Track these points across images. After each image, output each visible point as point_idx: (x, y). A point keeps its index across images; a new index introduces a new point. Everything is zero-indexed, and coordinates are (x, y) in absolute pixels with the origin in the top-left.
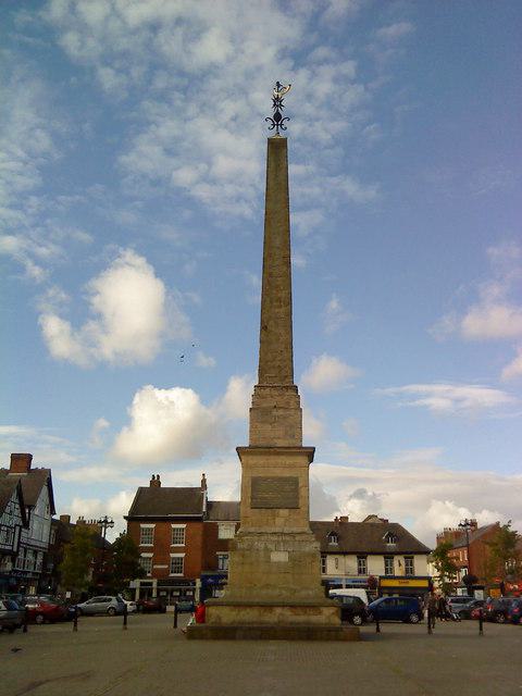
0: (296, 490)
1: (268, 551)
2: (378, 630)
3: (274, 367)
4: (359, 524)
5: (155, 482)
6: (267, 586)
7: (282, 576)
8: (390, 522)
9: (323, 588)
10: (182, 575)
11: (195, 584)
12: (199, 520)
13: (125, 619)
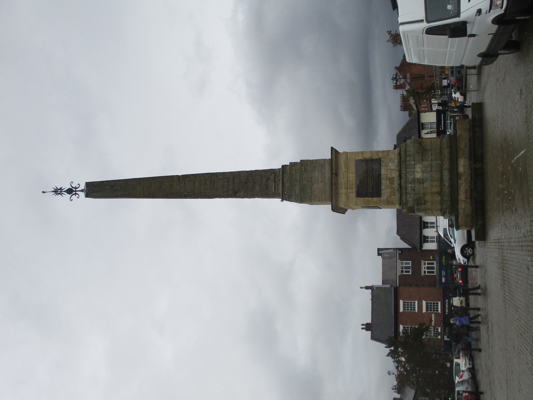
4: (406, 60)
5: (368, 327)
8: (400, 237)
12: (396, 289)
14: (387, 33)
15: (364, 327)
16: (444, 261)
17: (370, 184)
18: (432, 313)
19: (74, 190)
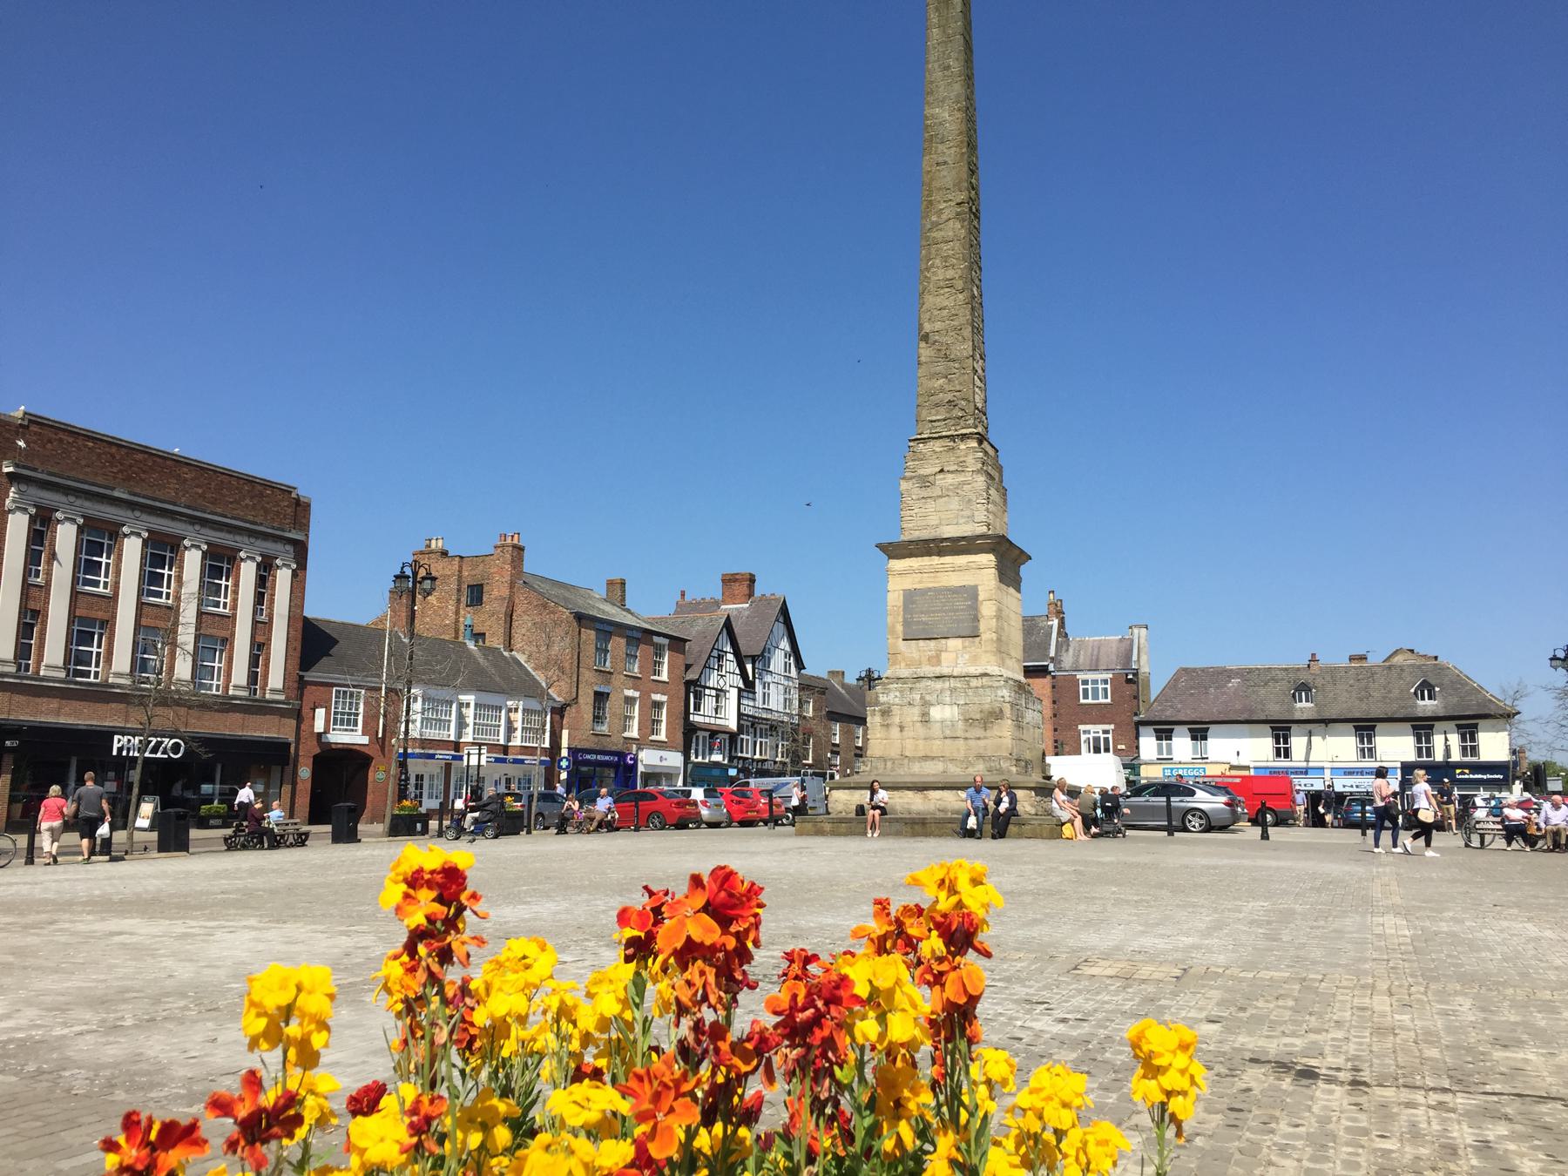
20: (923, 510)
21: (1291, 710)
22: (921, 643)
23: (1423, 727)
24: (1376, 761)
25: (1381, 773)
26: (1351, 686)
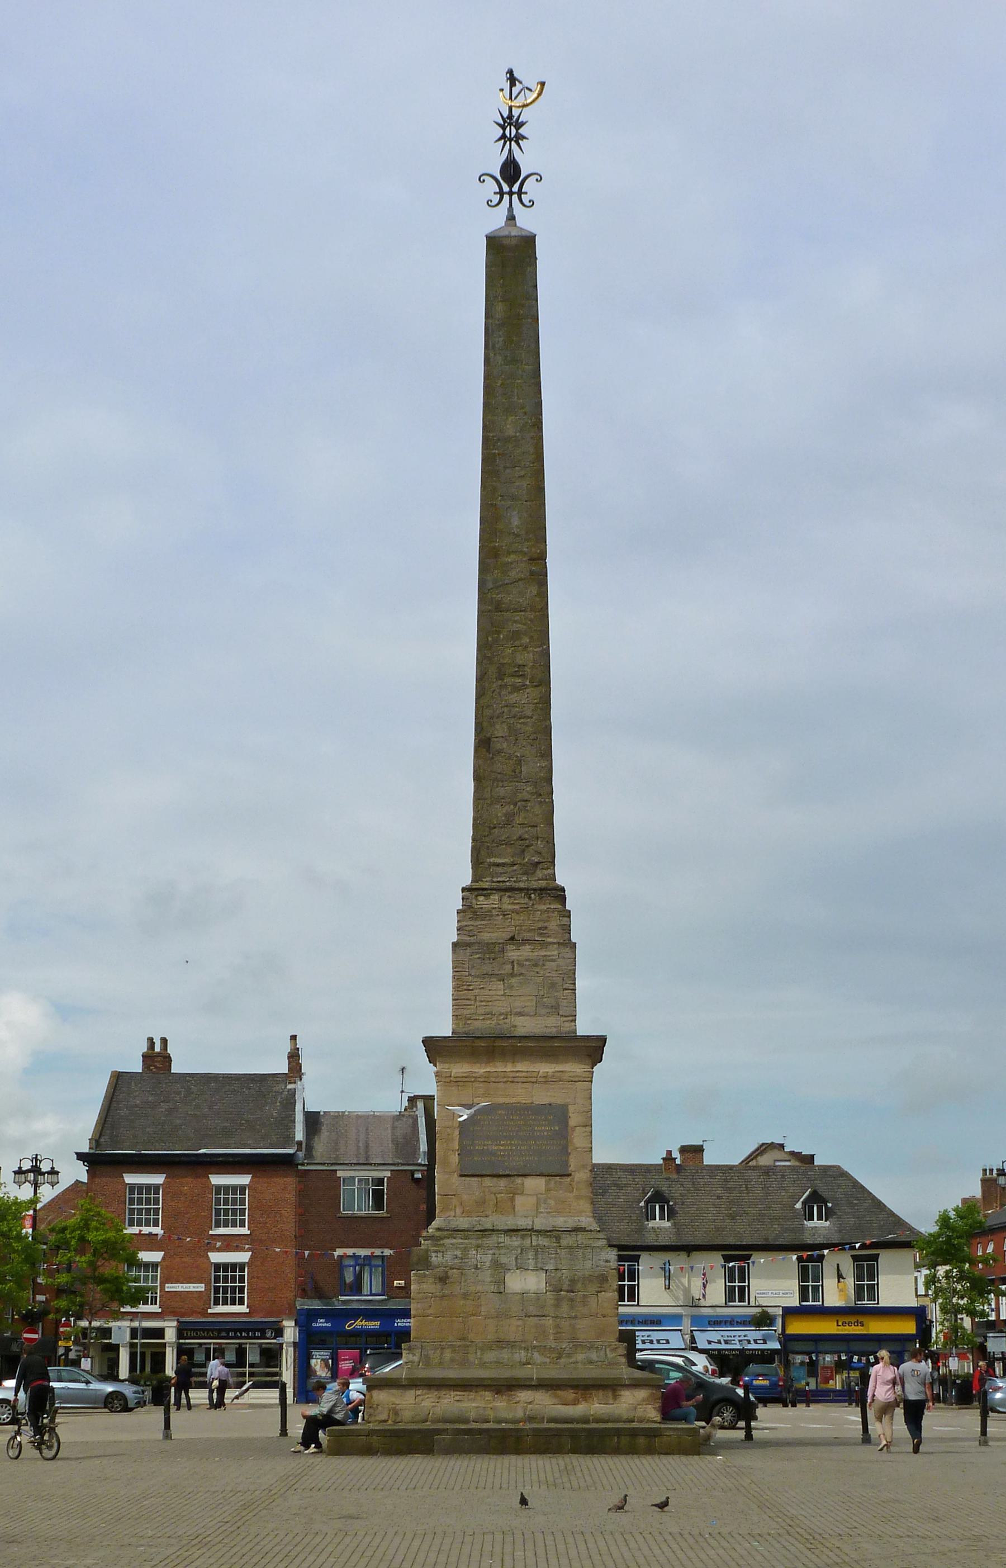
0: (563, 1133)
1: (499, 1268)
2: (90, 1323)
3: (508, 843)
6: (501, 1343)
7: (532, 1321)
9: (622, 1348)
10: (243, 1309)
11: (279, 1332)
12: (286, 1162)
13: (19, 1429)
14: (660, 1270)
15: (157, 1049)
16: (360, 1324)
17: (497, 1145)
18: (208, 1284)
19: (515, 188)
20: (487, 992)
21: (641, 1230)
22: (488, 1182)
23: (810, 1259)
24: (749, 1306)
25: (763, 1320)
26: (719, 1197)
